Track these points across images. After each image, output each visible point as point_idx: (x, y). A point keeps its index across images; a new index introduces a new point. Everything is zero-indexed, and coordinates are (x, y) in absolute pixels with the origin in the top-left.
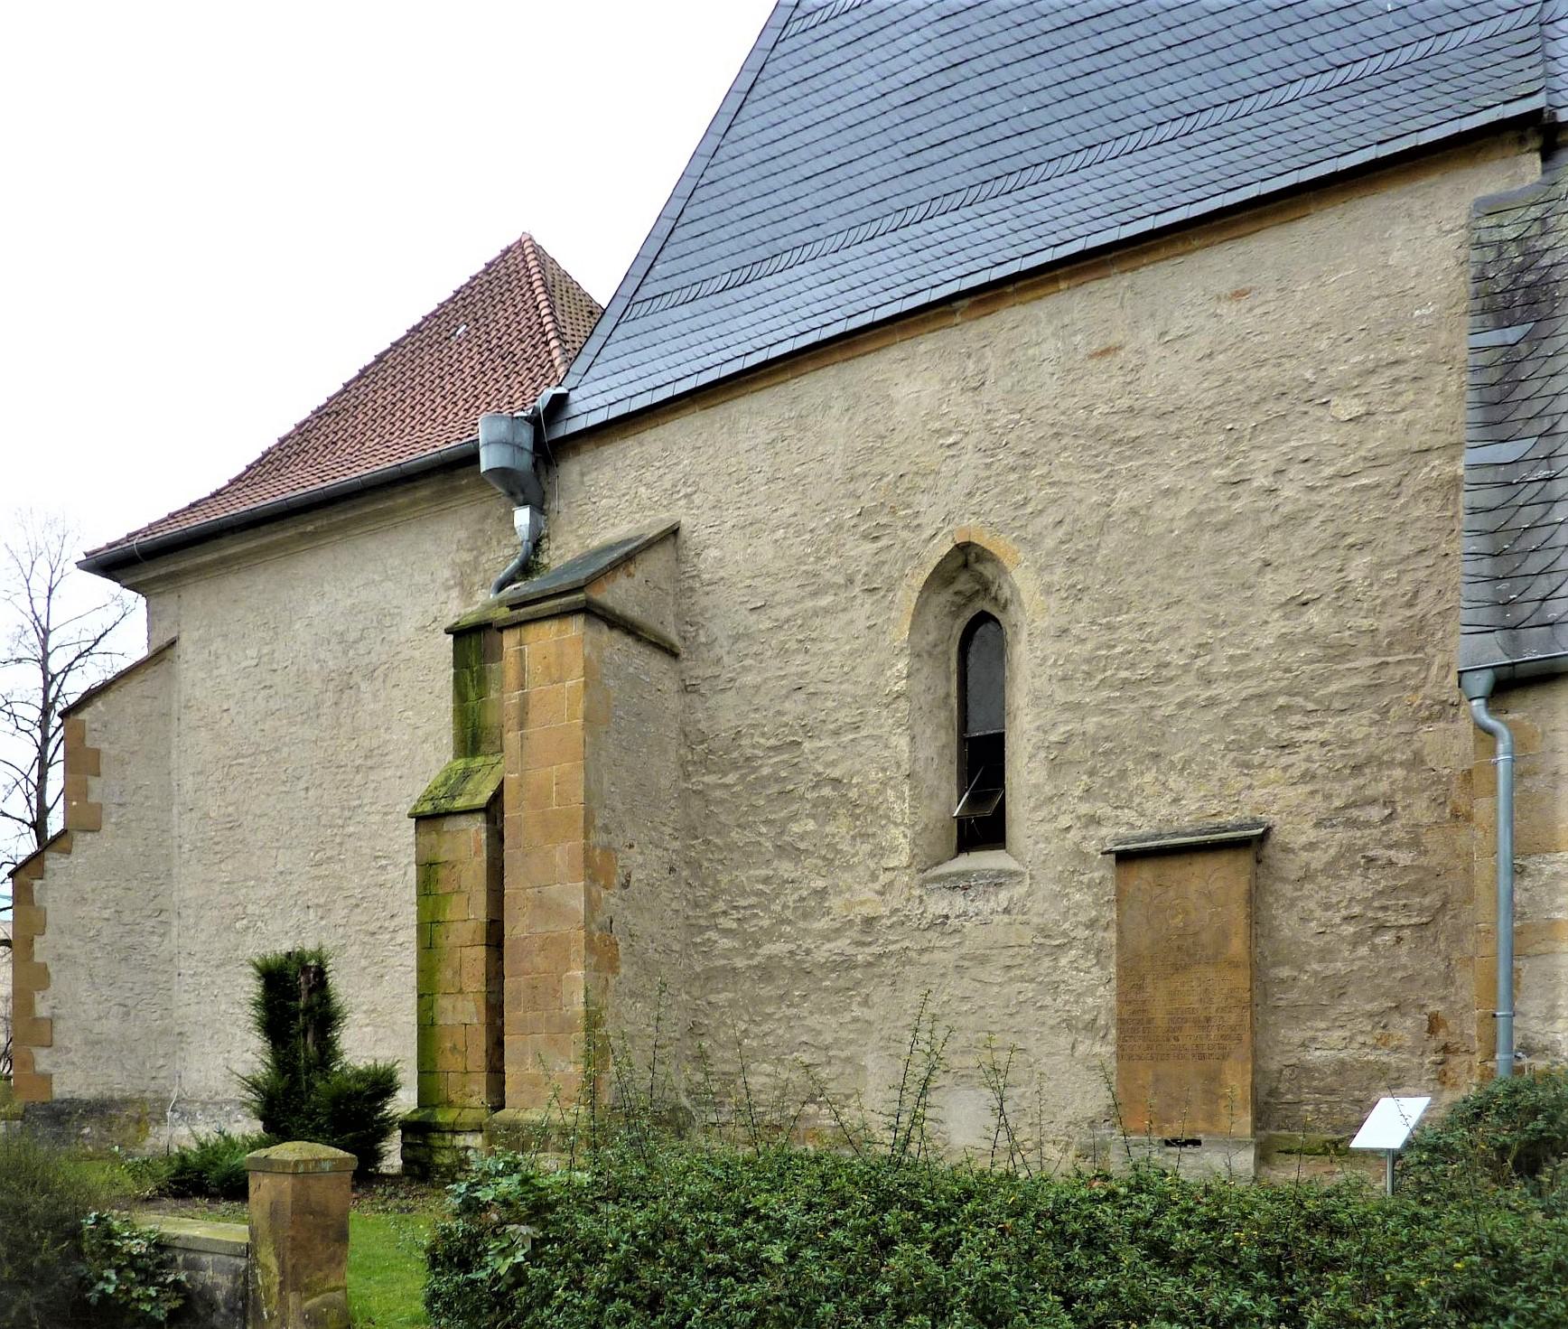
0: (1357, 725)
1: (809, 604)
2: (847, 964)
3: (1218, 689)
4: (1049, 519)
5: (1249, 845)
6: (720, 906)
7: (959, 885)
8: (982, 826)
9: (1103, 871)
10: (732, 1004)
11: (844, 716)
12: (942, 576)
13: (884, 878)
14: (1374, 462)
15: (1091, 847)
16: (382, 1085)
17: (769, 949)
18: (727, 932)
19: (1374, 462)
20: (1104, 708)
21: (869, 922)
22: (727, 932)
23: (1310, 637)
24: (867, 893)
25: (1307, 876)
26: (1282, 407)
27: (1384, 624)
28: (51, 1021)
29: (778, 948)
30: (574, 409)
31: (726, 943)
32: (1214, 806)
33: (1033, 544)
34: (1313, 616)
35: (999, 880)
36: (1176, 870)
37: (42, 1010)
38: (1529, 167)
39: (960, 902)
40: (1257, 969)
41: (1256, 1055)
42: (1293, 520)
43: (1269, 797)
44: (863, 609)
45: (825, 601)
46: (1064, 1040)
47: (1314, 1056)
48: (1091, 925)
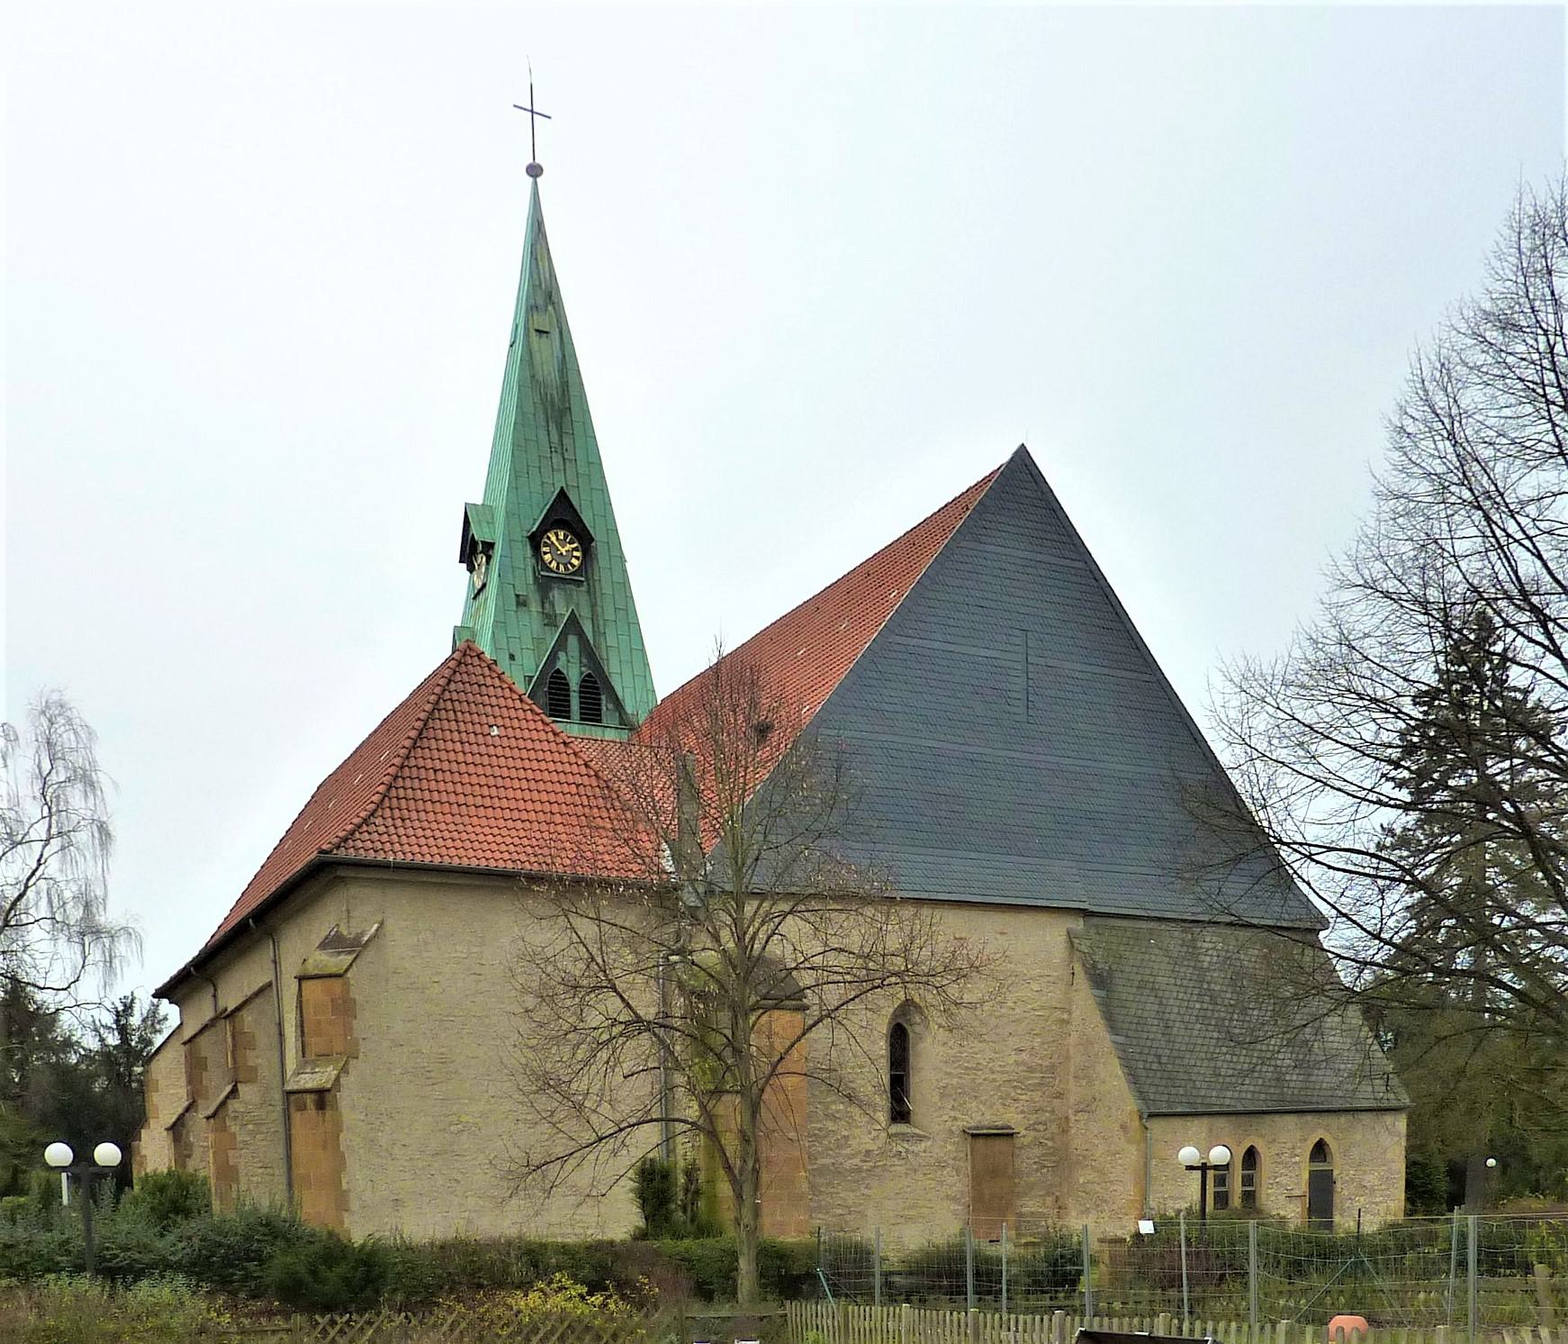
0: (1036, 1096)
2: (859, 1170)
7: (904, 1137)
8: (900, 1114)
14: (1042, 1008)
17: (821, 1161)
19: (1042, 1008)
21: (868, 1152)
29: (828, 1161)
36: (990, 1141)
43: (1012, 1117)
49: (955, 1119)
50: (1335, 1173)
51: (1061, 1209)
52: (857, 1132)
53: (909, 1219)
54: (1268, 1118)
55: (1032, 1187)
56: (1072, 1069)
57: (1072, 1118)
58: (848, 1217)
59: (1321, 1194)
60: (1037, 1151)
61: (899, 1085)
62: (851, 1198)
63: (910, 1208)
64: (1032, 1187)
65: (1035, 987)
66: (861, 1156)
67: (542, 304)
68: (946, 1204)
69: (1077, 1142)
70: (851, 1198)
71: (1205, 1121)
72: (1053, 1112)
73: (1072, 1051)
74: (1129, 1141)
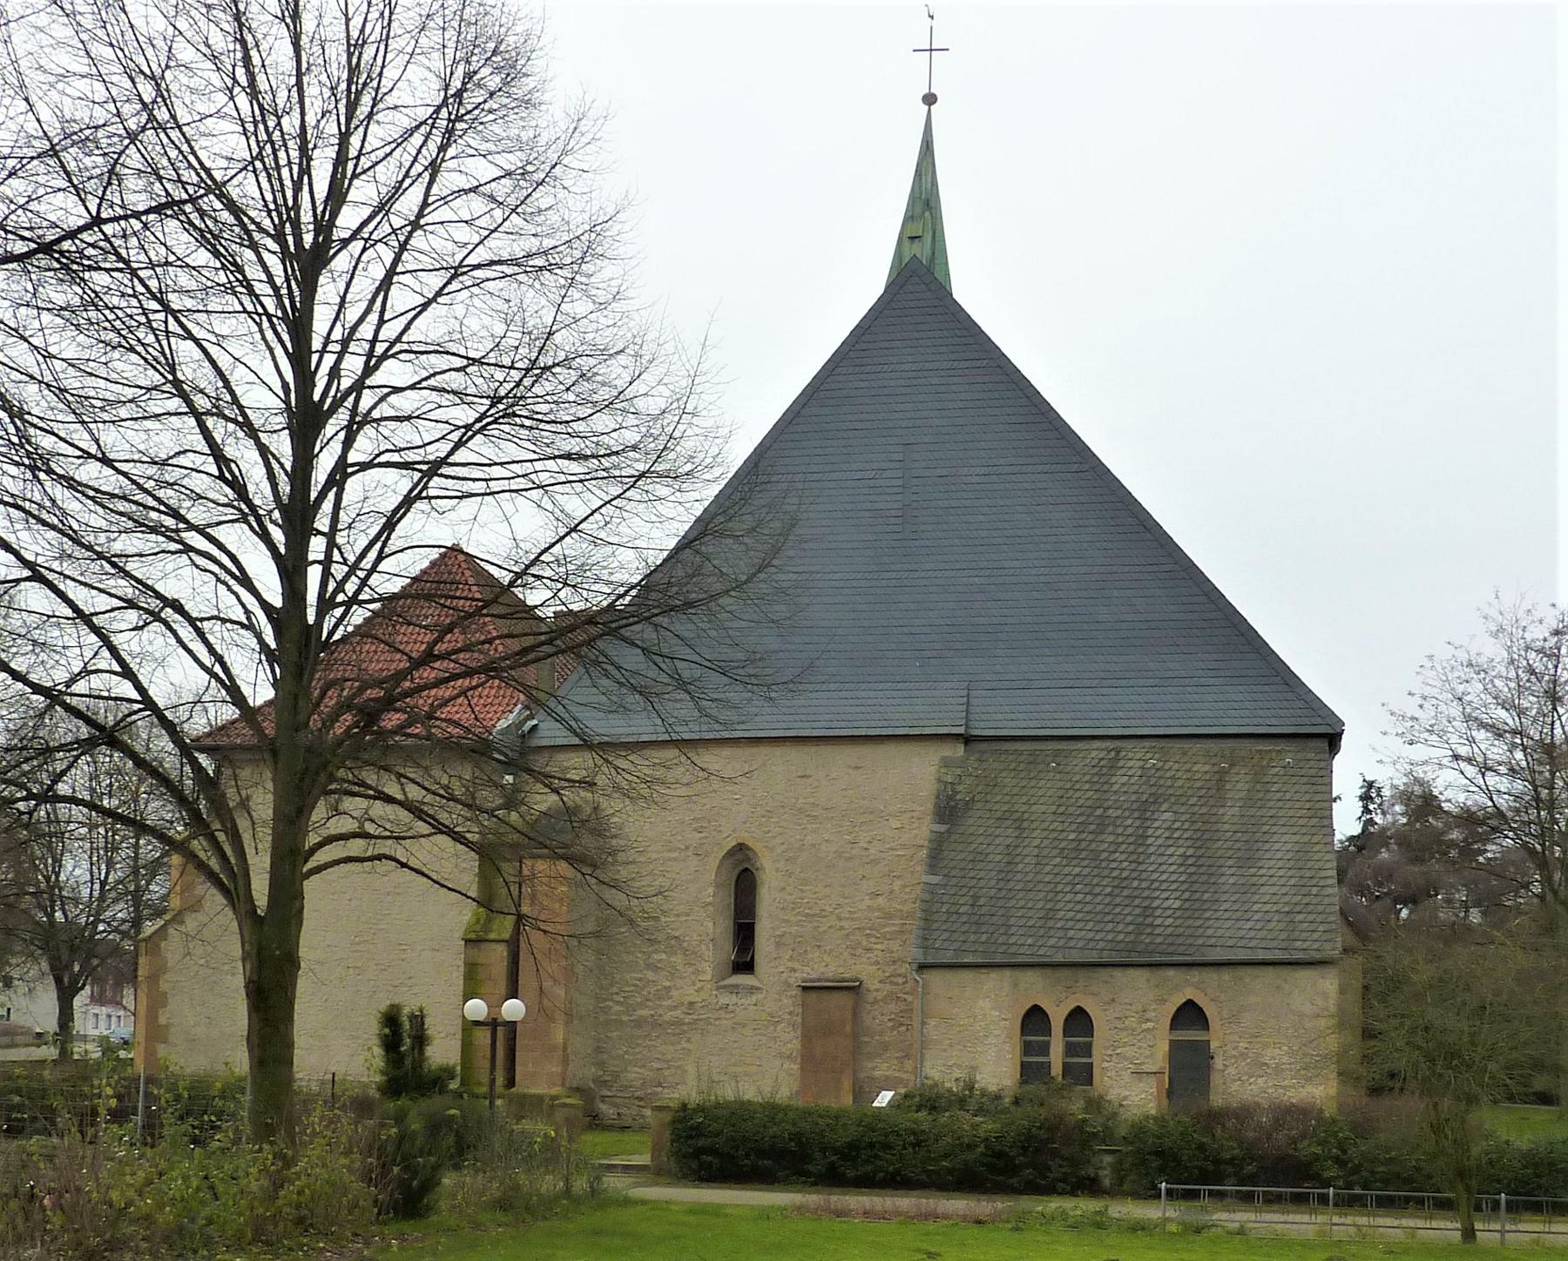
0: (895, 945)
1: (666, 855)
2: (679, 1023)
3: (843, 923)
4: (779, 841)
5: (853, 989)
6: (615, 990)
7: (734, 990)
8: (744, 965)
9: (797, 992)
10: (620, 1038)
11: (681, 909)
12: (731, 853)
13: (699, 985)
14: (904, 846)
15: (792, 980)
16: (449, 1073)
17: (640, 1012)
18: (618, 1003)
19: (904, 846)
20: (798, 923)
21: (691, 1004)
22: (618, 1003)
23: (879, 909)
24: (691, 990)
25: (876, 1001)
26: (871, 817)
27: (906, 908)
28: (167, 1026)
29: (645, 1012)
30: (541, 733)
31: (618, 1008)
32: (841, 970)
33: (772, 850)
34: (880, 900)
35: (752, 990)
36: (826, 995)
37: (162, 1020)
38: (960, 750)
39: (734, 999)
40: (855, 1036)
41: (855, 1072)
42: (874, 862)
43: (864, 969)
44: (693, 862)
45: (674, 855)
46: (778, 1063)
47: (877, 1073)
48: (790, 1013)
50: (1214, 1045)
52: (679, 983)
54: (1103, 973)
59: (1190, 1064)
63: (735, 1065)
64: (886, 1047)
67: (924, 205)
71: (1007, 973)
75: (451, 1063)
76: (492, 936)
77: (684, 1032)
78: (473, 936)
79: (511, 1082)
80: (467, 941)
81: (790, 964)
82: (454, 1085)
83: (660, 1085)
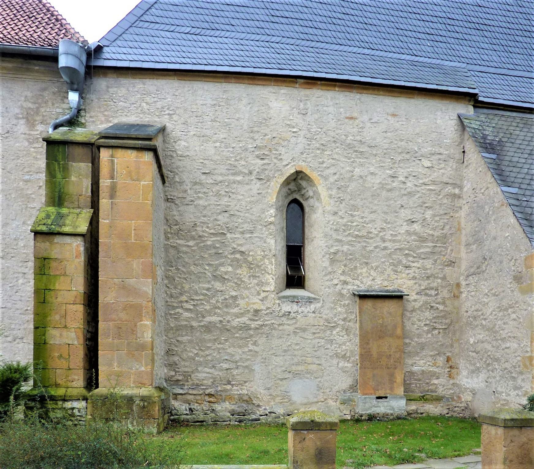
0: (428, 264)
1: (231, 178)
2: (247, 328)
3: (387, 244)
4: (332, 170)
6: (184, 298)
7: (294, 300)
8: (295, 279)
10: (190, 342)
11: (246, 227)
12: (287, 182)
13: (263, 295)
14: (434, 182)
15: (345, 292)
17: (208, 319)
18: (187, 310)
19: (434, 182)
20: (349, 243)
21: (257, 311)
22: (187, 310)
24: (256, 300)
25: (414, 310)
26: (408, 156)
29: (214, 319)
31: (187, 314)
32: (386, 283)
33: (326, 178)
34: (416, 227)
36: (379, 303)
39: (295, 307)
43: (401, 283)
44: (256, 186)
45: (239, 178)
47: (415, 369)
48: (344, 320)
49: (345, 283)
51: (452, 368)
53: (297, 375)
55: (423, 347)
56: (464, 239)
57: (464, 283)
58: (235, 372)
60: (428, 314)
61: (295, 255)
62: (238, 353)
63: (297, 364)
64: (423, 347)
65: (427, 163)
66: (250, 316)
68: (335, 361)
69: (468, 303)
70: (238, 353)
72: (444, 278)
73: (463, 221)
74: (523, 292)
75: (23, 364)
76: (66, 229)
77: (251, 336)
78: (44, 228)
79: (92, 382)
80: (37, 233)
81: (342, 278)
82: (26, 387)
83: (229, 383)
